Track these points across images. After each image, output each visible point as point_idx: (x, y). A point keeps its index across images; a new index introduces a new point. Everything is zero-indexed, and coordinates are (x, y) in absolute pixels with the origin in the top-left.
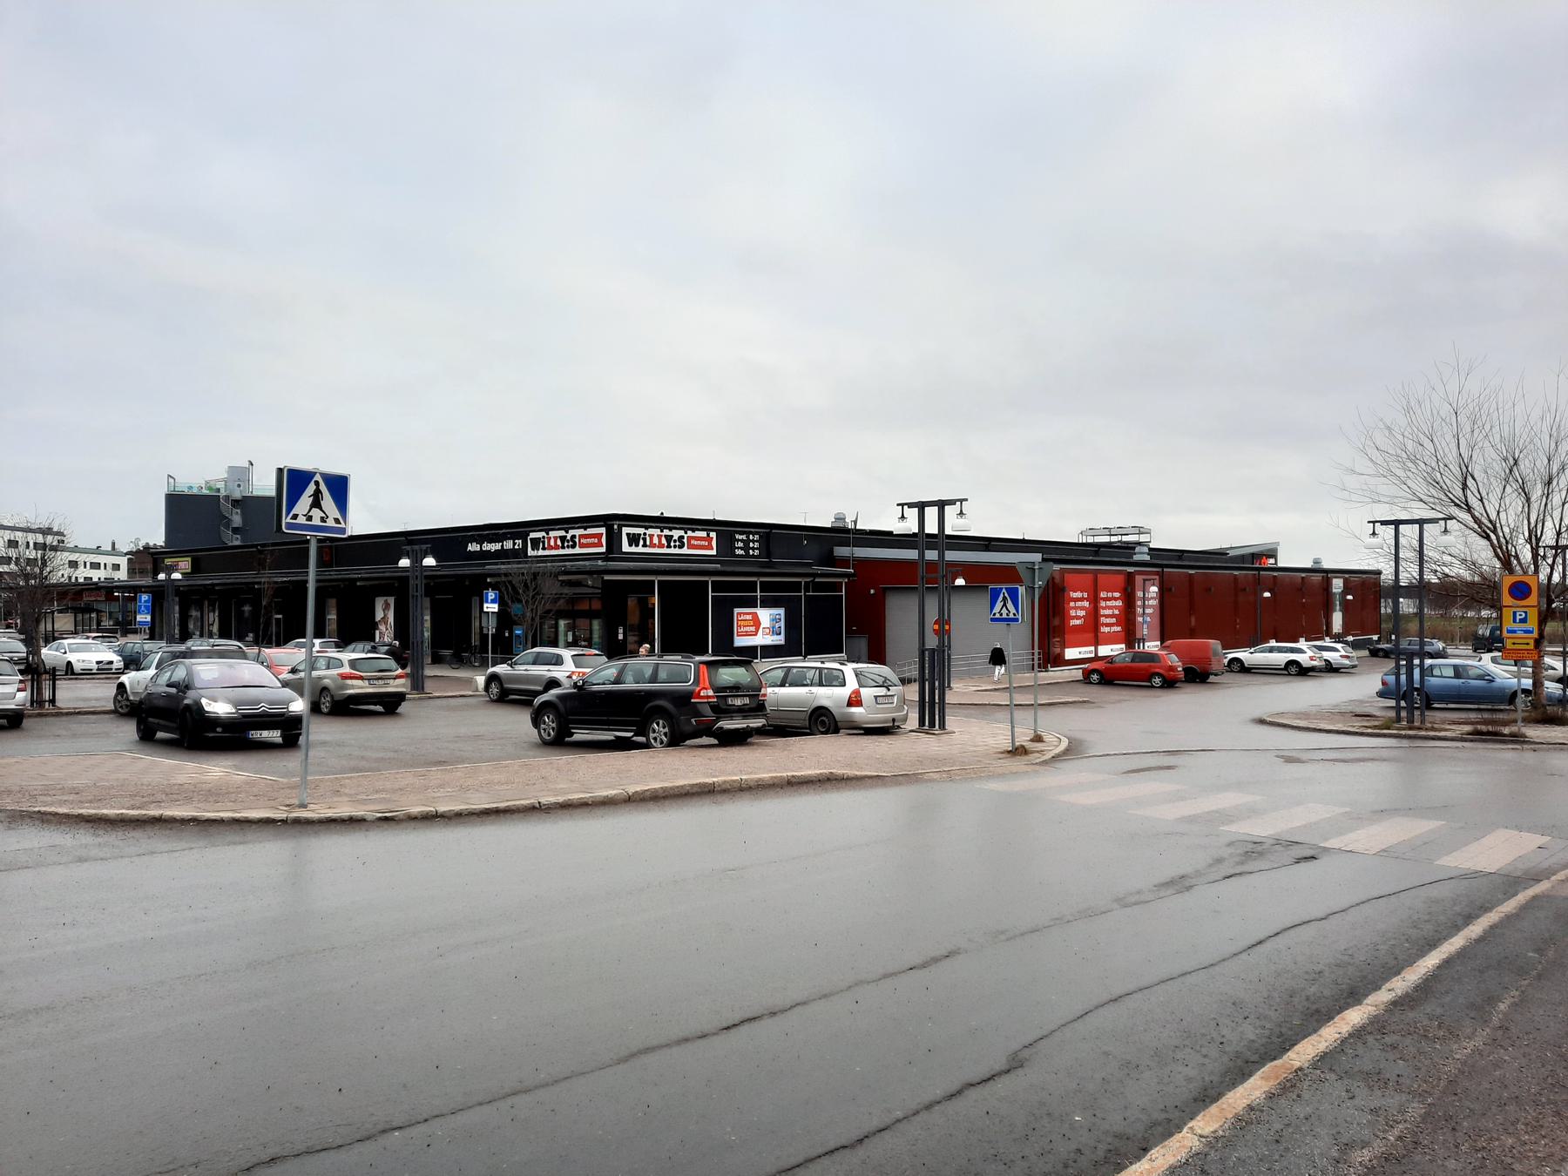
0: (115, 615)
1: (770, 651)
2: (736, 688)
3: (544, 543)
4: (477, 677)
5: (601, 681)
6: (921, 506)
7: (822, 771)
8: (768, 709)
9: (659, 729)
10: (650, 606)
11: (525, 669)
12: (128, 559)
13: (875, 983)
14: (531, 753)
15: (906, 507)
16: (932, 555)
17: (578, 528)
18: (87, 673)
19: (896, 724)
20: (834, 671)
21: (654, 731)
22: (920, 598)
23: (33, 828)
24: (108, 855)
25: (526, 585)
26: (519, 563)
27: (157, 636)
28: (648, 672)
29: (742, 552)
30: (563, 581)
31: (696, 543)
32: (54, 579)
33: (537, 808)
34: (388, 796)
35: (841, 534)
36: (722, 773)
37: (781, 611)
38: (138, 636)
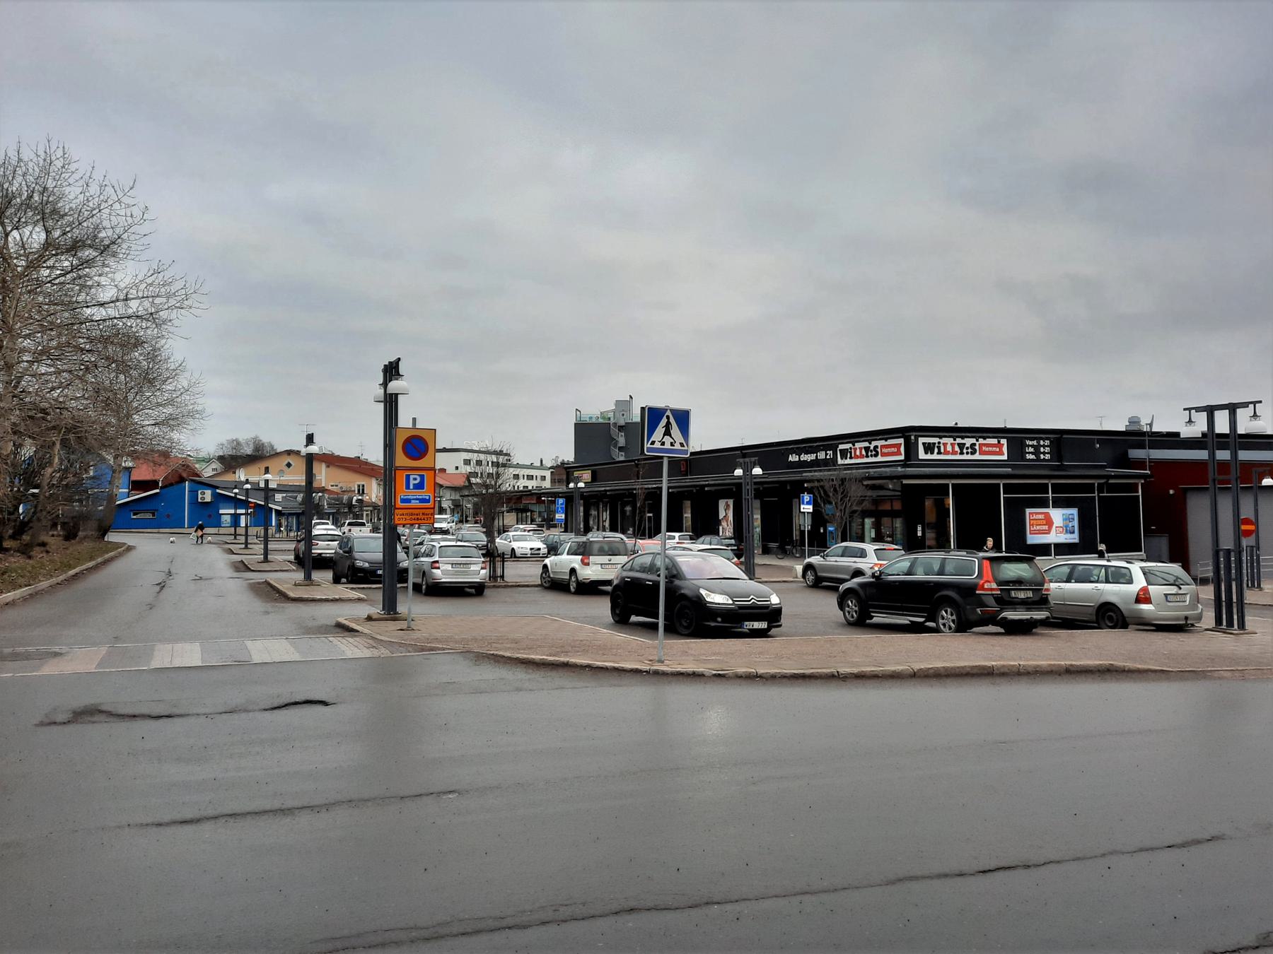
0: (542, 514)
1: (1063, 549)
2: (1019, 582)
3: (851, 453)
4: (797, 566)
5: (896, 573)
6: (1210, 411)
7: (1101, 663)
8: (1052, 602)
9: (947, 616)
10: (947, 506)
11: (834, 560)
12: (552, 472)
13: (1131, 854)
14: (836, 631)
15: (1193, 411)
16: (1224, 455)
17: (880, 439)
18: (524, 557)
19: (1189, 622)
20: (1123, 569)
21: (943, 618)
22: (1233, 497)
23: (489, 666)
24: (535, 688)
25: (835, 490)
26: (829, 470)
27: (569, 530)
28: (936, 568)
29: (1032, 457)
30: (867, 486)
31: (987, 449)
32: (503, 489)
33: (836, 676)
34: (721, 658)
35: (1135, 437)
36: (1002, 658)
37: (1074, 511)
38: (557, 529)
